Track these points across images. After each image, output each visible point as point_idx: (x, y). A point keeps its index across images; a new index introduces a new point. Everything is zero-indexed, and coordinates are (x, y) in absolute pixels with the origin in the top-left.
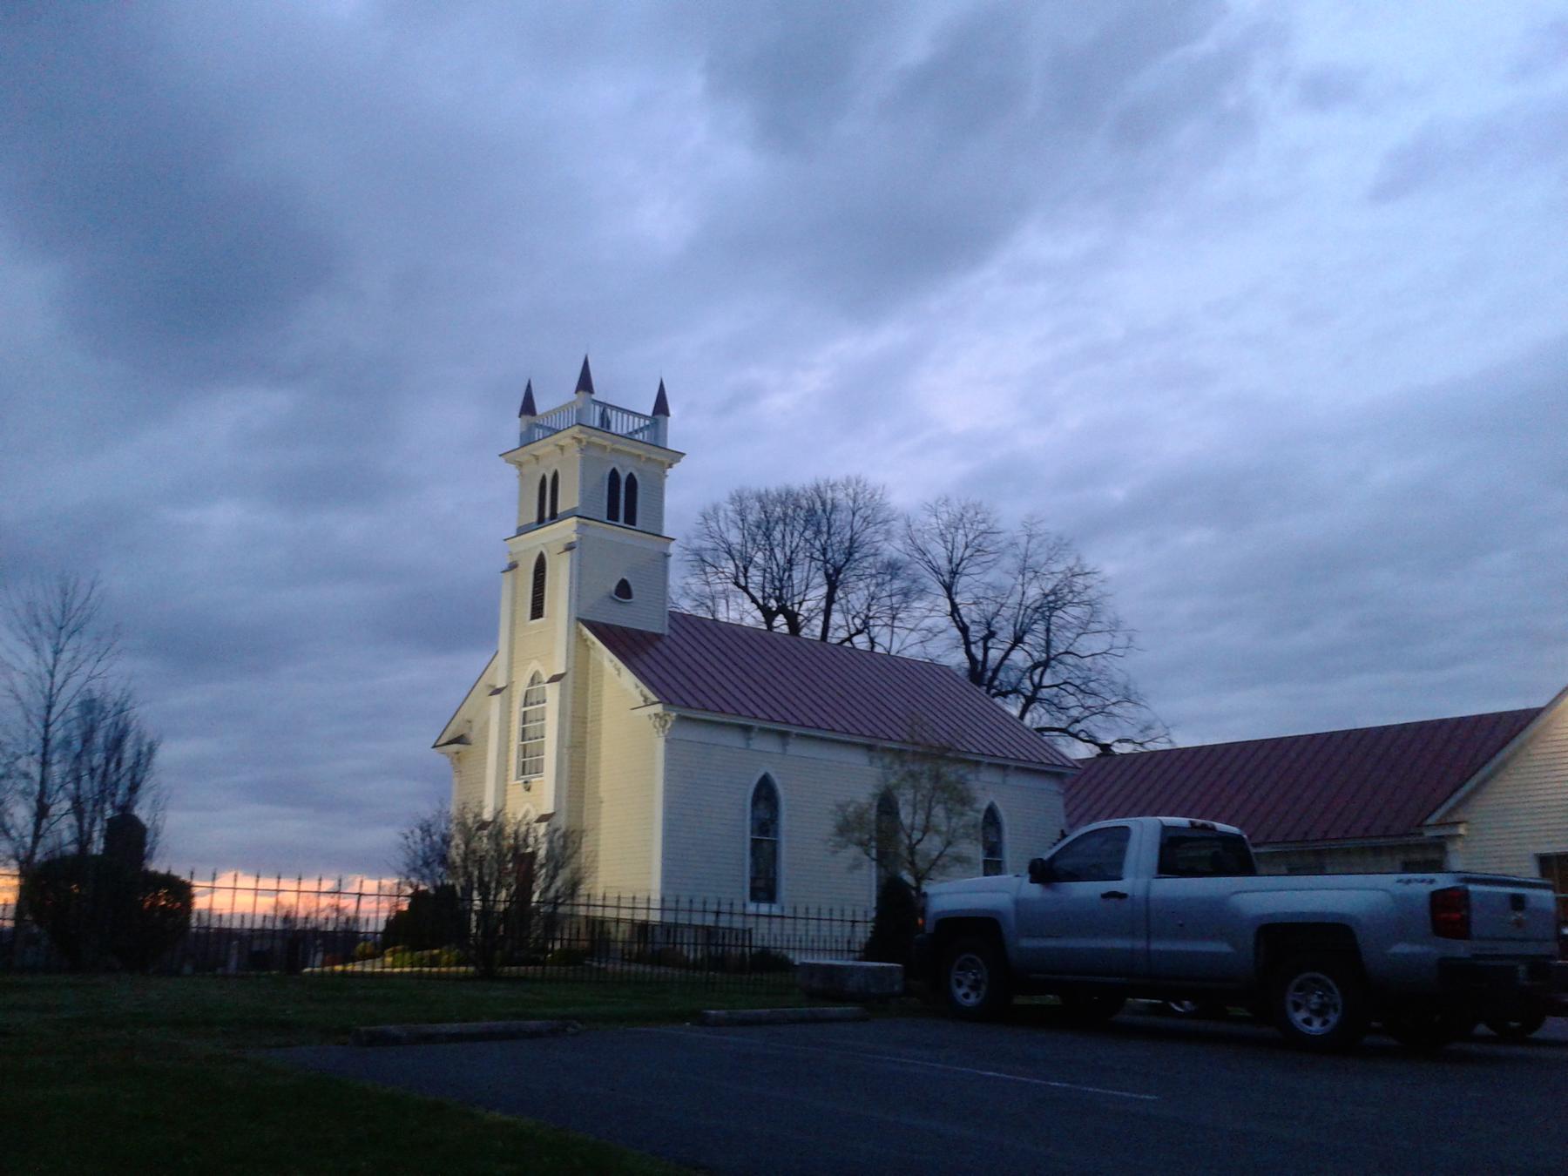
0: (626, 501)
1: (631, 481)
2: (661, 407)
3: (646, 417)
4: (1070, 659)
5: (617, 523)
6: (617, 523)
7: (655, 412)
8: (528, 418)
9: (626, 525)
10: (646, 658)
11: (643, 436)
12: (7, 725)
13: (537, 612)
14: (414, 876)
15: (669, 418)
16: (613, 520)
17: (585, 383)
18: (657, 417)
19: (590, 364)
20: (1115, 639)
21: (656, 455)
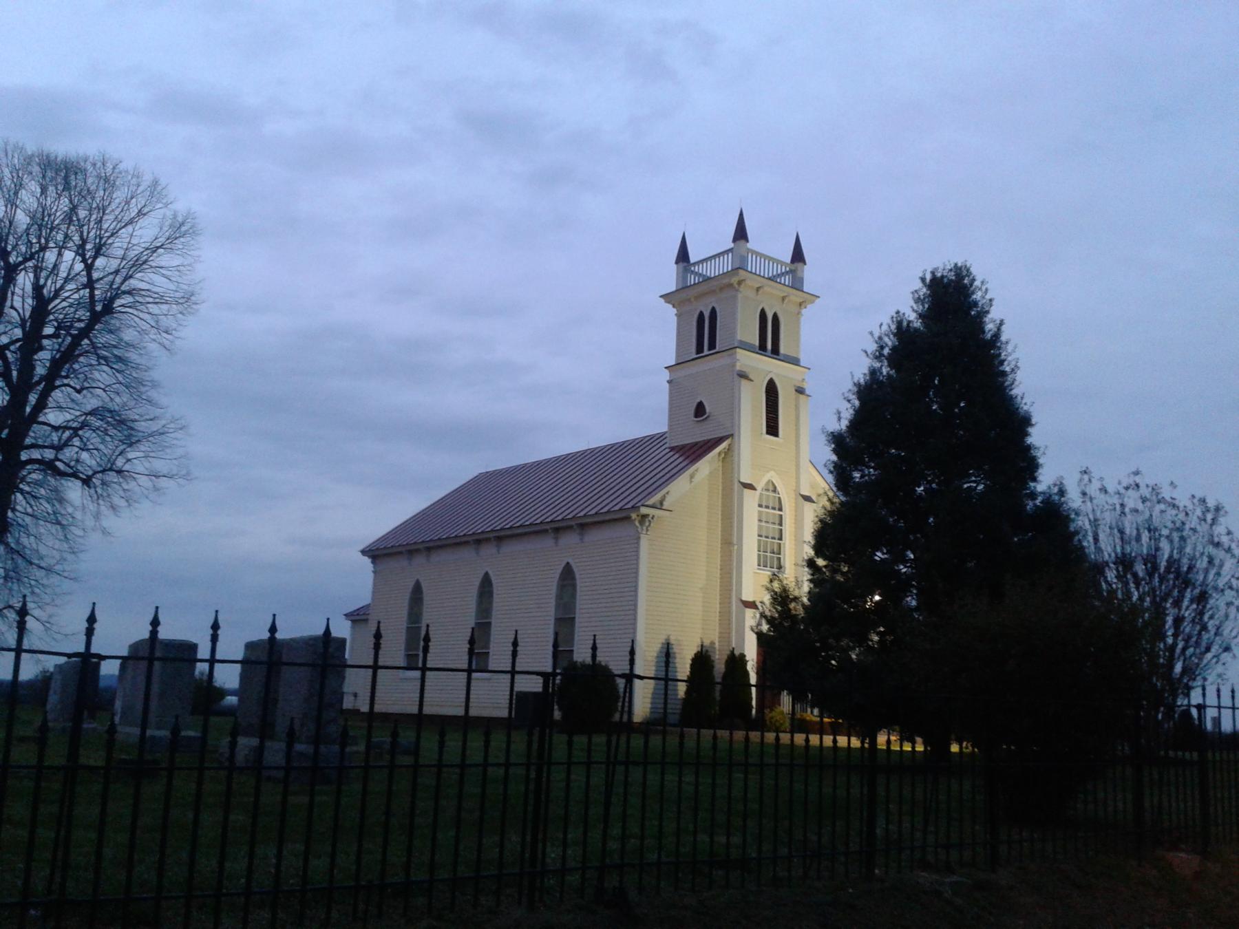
0: (704, 323)
1: (776, 318)
2: (798, 256)
3: (782, 263)
4: (79, 493)
5: (766, 354)
6: (766, 354)
7: (793, 261)
8: (681, 265)
9: (772, 356)
10: (681, 459)
11: (785, 280)
12: (1185, 507)
13: (773, 429)
14: (1092, 559)
15: (805, 267)
16: (775, 354)
17: (741, 233)
18: (796, 264)
19: (801, 239)
20: (1100, 486)
21: (795, 296)
